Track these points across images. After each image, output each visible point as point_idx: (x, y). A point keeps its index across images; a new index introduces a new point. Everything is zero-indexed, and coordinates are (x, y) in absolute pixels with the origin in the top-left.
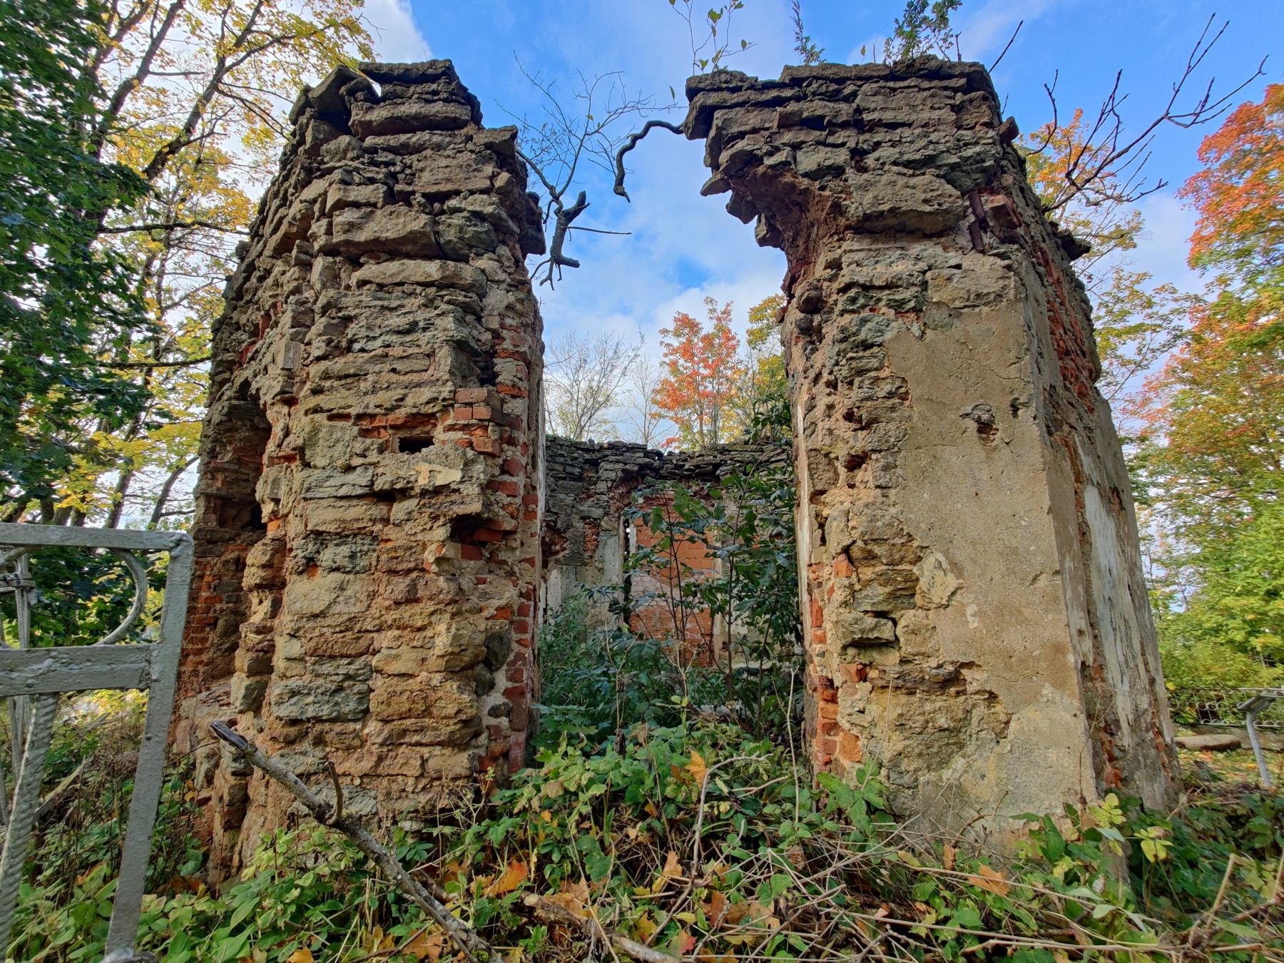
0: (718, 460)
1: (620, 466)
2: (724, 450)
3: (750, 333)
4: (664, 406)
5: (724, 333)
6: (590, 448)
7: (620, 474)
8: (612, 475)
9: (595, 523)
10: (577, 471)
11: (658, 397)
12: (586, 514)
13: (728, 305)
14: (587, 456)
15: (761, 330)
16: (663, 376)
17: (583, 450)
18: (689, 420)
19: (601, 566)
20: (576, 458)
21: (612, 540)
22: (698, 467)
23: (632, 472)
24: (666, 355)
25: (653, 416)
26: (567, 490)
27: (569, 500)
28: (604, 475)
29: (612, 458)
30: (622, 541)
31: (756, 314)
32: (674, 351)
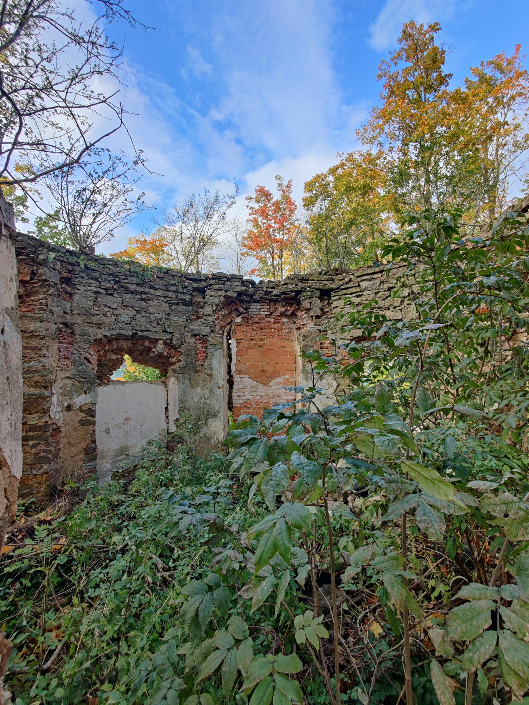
0: (299, 287)
1: (223, 293)
2: (304, 280)
3: (304, 200)
4: (250, 248)
5: (286, 199)
6: (197, 279)
7: (223, 300)
8: (216, 300)
9: (204, 339)
10: (187, 297)
11: (246, 242)
12: (196, 332)
13: (290, 181)
14: (195, 285)
15: (312, 197)
16: (248, 229)
17: (192, 280)
18: (265, 257)
19: (209, 372)
20: (186, 287)
21: (218, 352)
22: (284, 293)
23: (232, 298)
24: (250, 214)
25: (243, 254)
26: (179, 314)
27: (182, 321)
28: (210, 300)
29: (215, 287)
30: (225, 352)
31: (309, 187)
32: (256, 212)
